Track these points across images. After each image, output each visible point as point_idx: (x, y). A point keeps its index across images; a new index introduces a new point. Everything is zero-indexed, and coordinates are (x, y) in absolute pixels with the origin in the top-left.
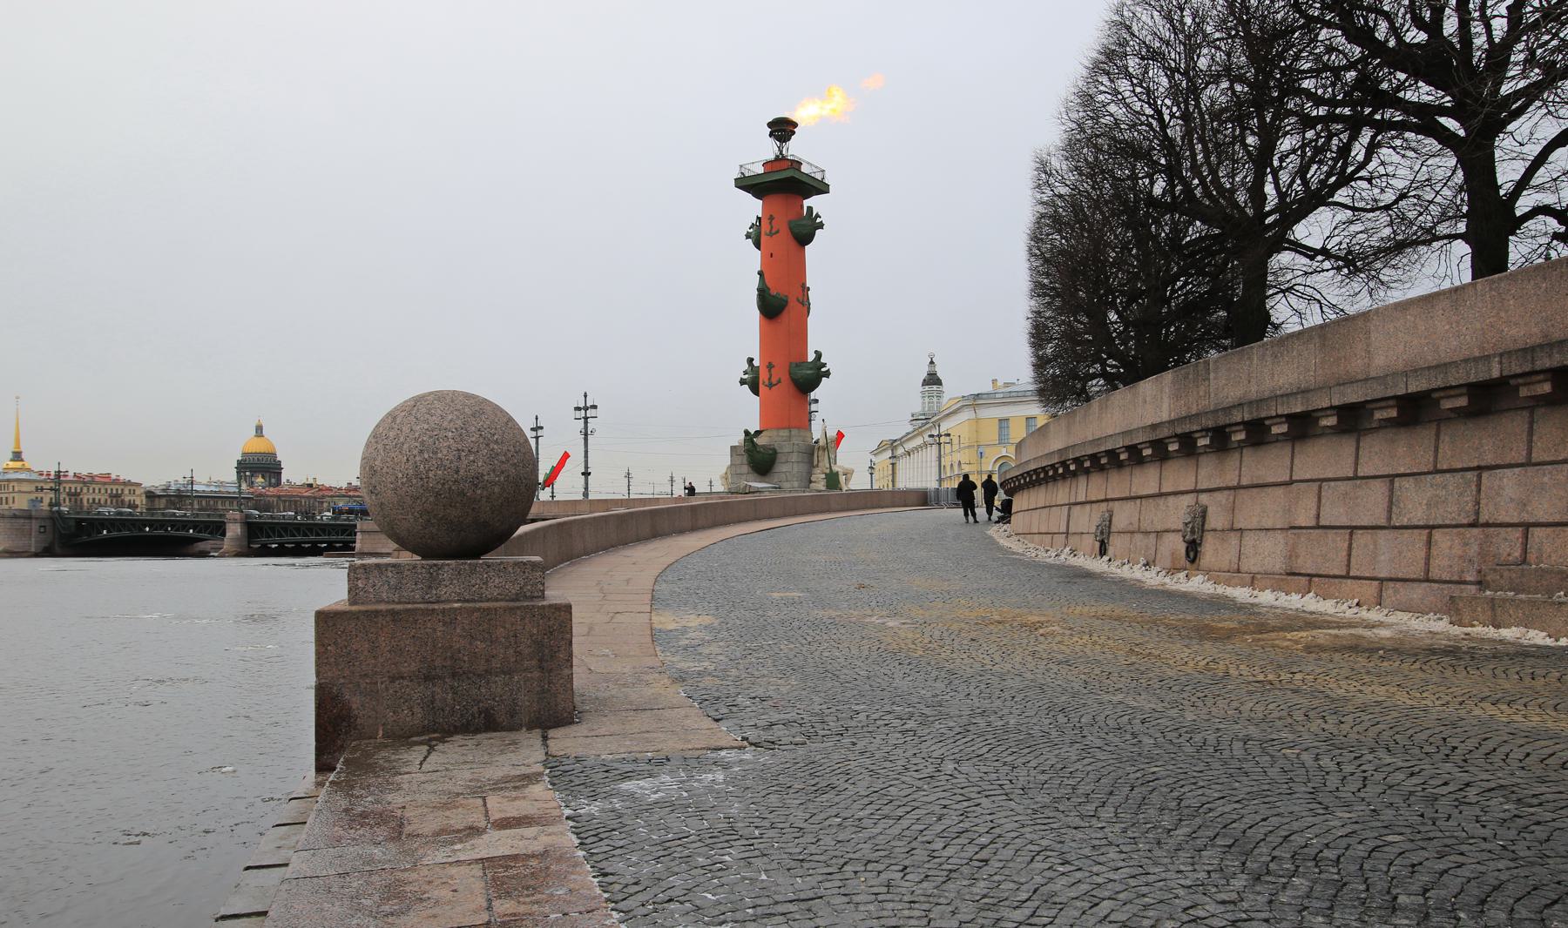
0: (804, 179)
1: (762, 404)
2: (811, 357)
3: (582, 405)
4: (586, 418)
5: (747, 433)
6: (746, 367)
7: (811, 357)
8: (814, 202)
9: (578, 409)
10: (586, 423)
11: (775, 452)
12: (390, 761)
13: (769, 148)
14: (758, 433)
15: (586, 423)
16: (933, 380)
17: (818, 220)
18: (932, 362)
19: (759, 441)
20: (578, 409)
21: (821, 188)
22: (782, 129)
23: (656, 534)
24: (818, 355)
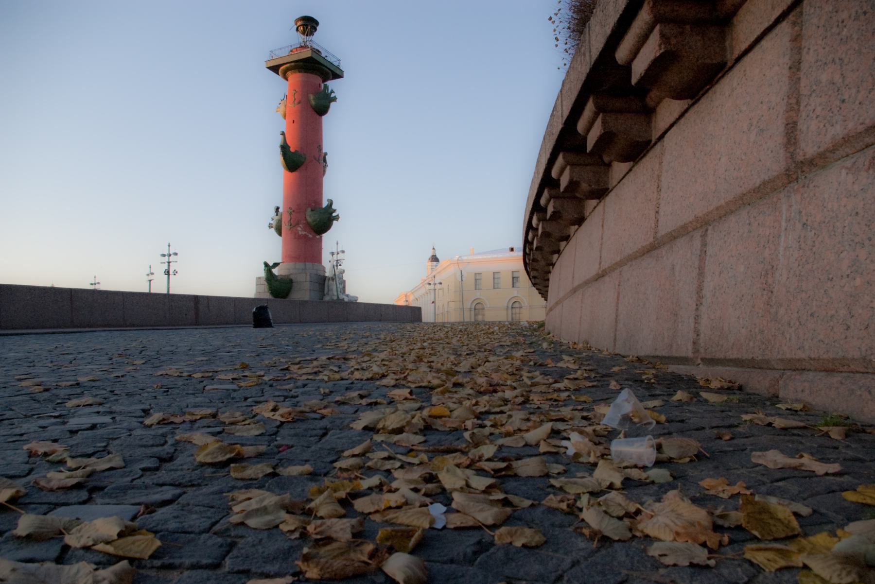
0: (322, 61)
1: (285, 244)
2: (325, 204)
3: (166, 253)
4: (169, 263)
5: (266, 265)
6: (273, 213)
7: (325, 204)
8: (332, 84)
9: (164, 255)
10: (169, 266)
11: (291, 281)
12: (598, 380)
13: (298, 38)
14: (276, 265)
15: (169, 266)
16: (435, 259)
17: (333, 95)
18: (434, 249)
19: (275, 271)
20: (164, 255)
21: (336, 74)
22: (308, 25)
23: (108, 325)
24: (331, 203)
